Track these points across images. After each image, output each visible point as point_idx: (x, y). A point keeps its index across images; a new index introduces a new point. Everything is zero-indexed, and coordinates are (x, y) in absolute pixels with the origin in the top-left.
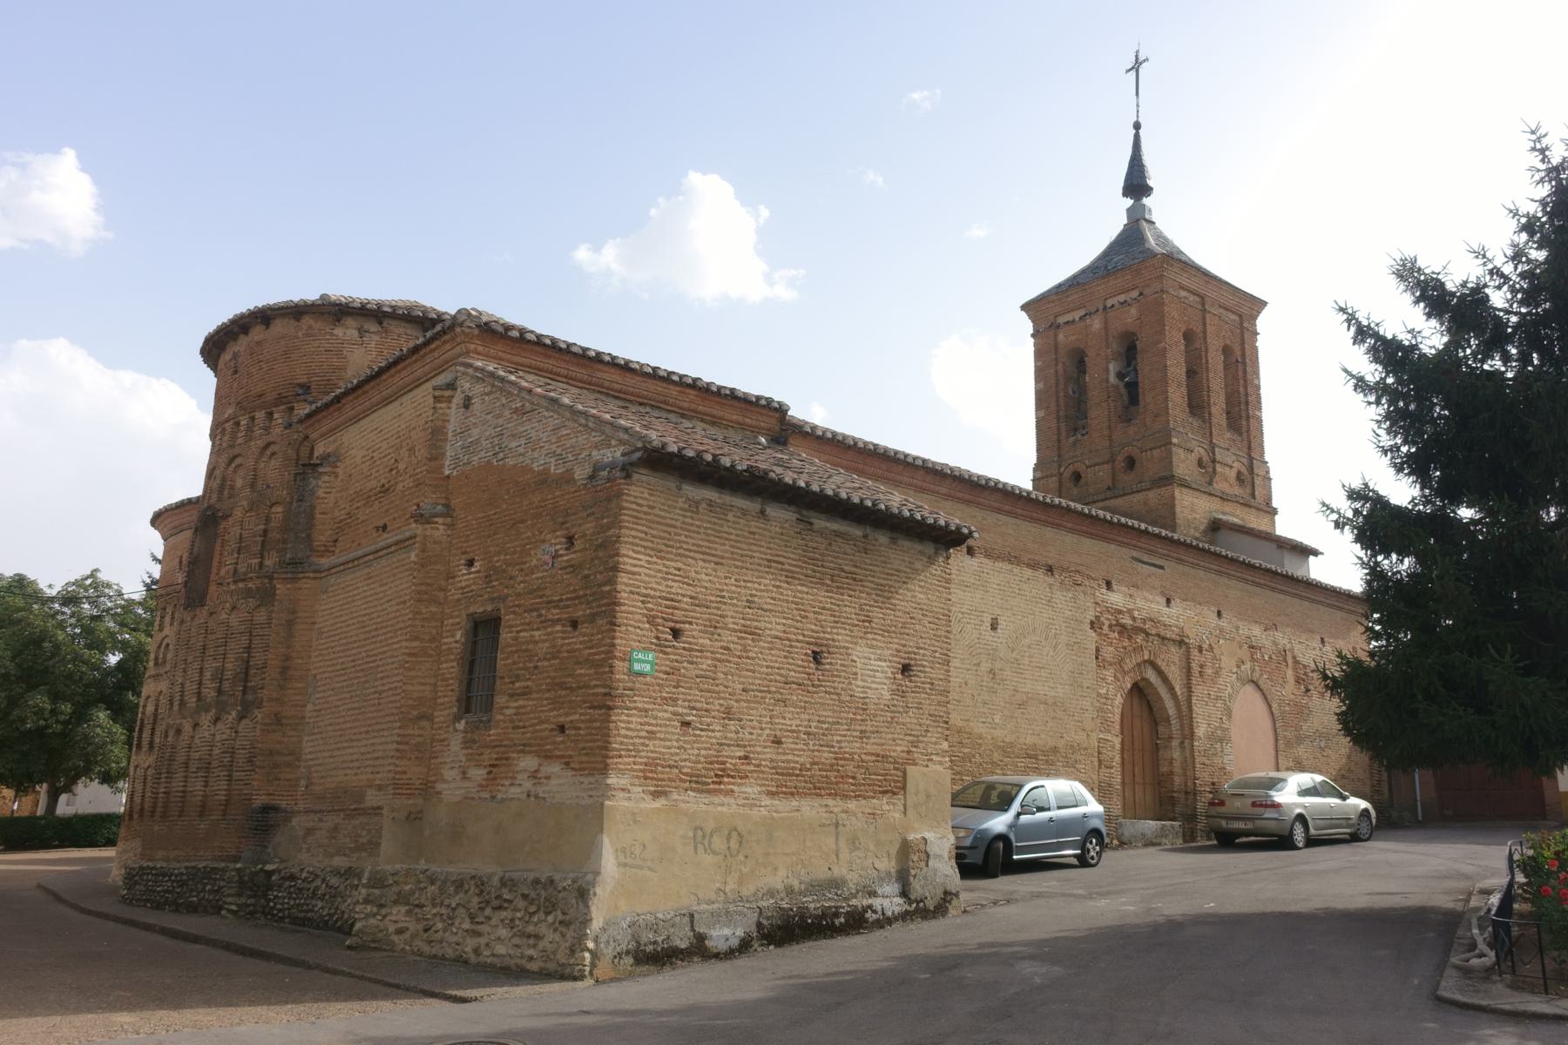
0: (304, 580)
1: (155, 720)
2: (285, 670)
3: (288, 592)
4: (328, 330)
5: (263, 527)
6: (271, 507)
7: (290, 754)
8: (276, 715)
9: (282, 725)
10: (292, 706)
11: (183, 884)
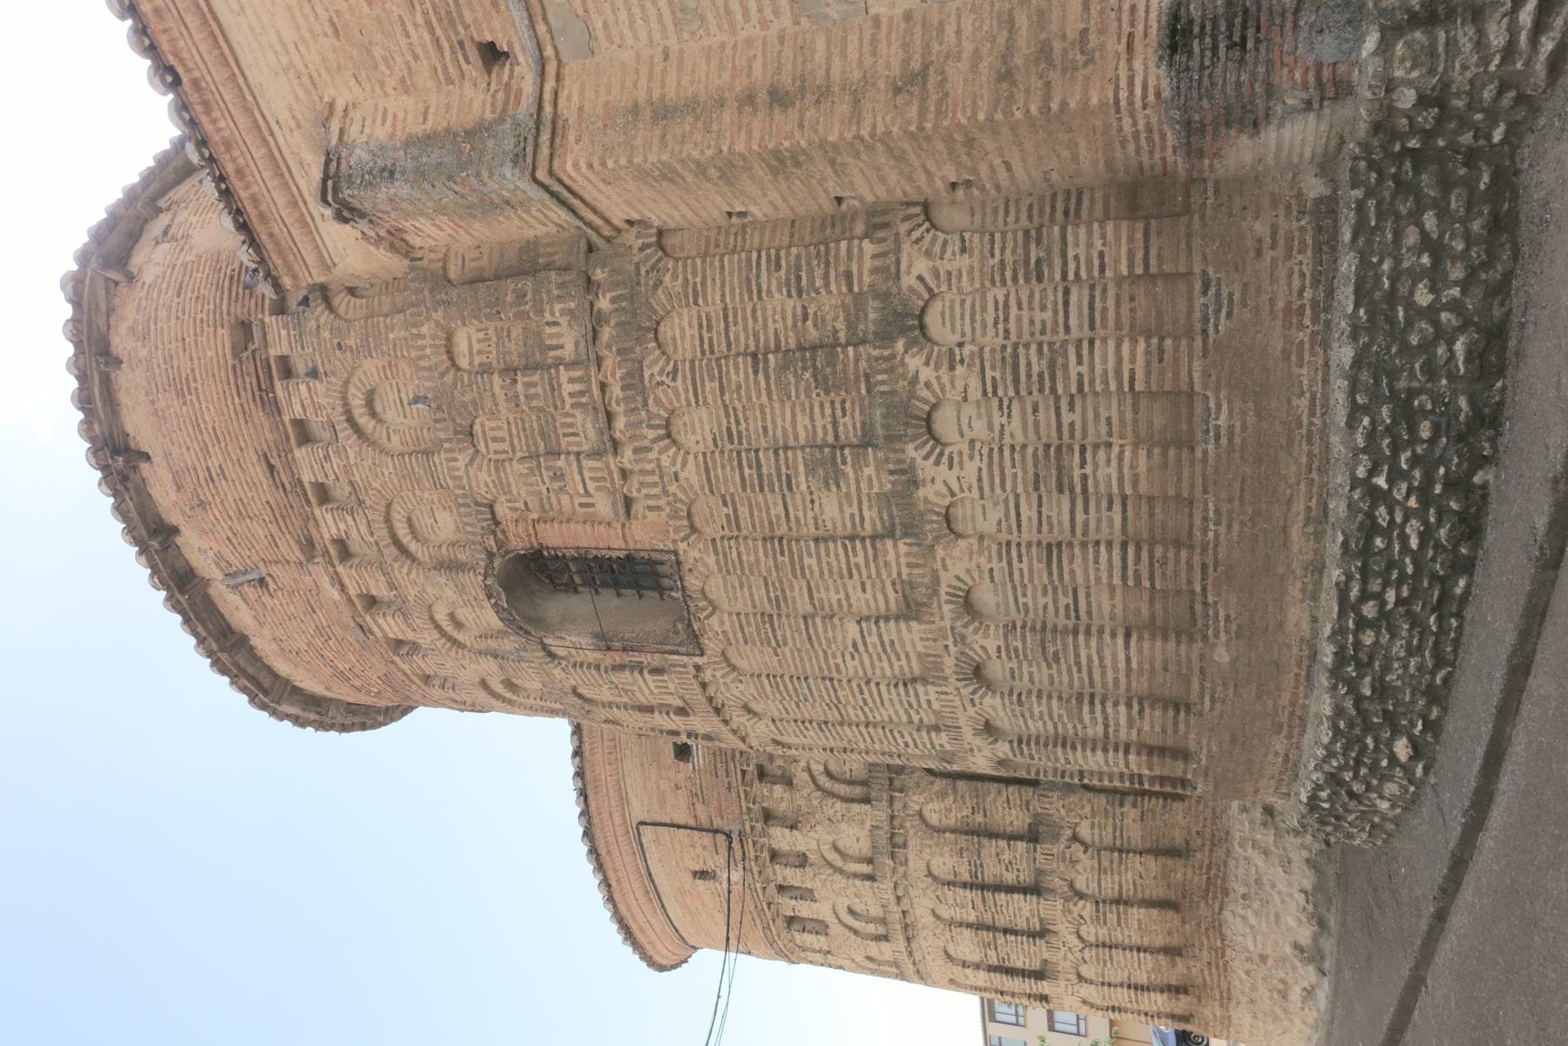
0: (562, 103)
1: (988, 928)
2: (779, 98)
3: (585, 138)
4: (143, 294)
5: (496, 378)
6: (459, 369)
7: (1011, 22)
8: (898, 91)
9: (926, 67)
10: (874, 53)
11: (1406, 414)
